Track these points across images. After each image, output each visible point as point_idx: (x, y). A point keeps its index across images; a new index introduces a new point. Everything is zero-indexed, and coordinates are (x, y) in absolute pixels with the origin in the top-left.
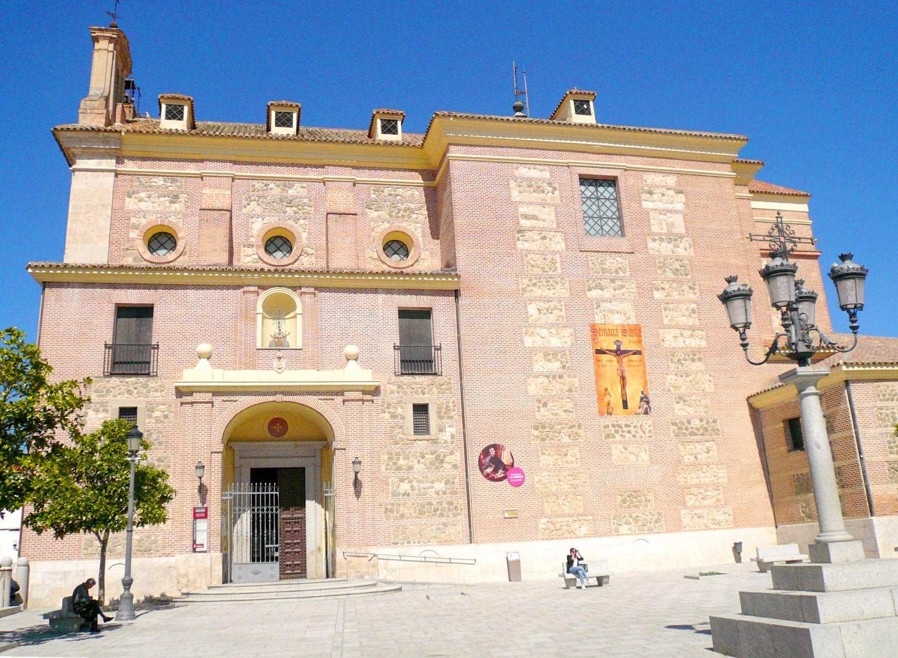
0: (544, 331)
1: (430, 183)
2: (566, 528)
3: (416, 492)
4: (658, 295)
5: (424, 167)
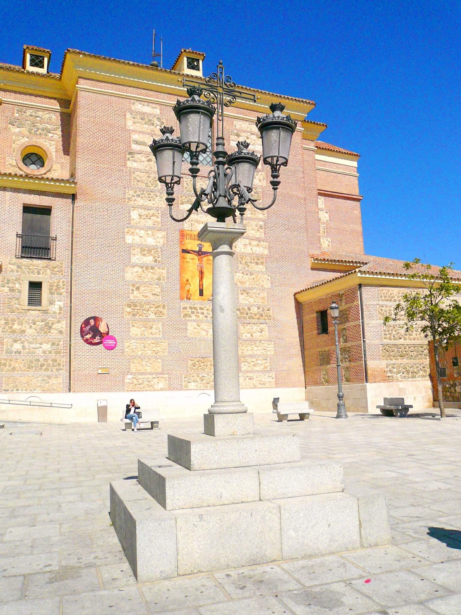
1: (65, 110)
2: (146, 383)
3: (27, 350)
5: (64, 97)
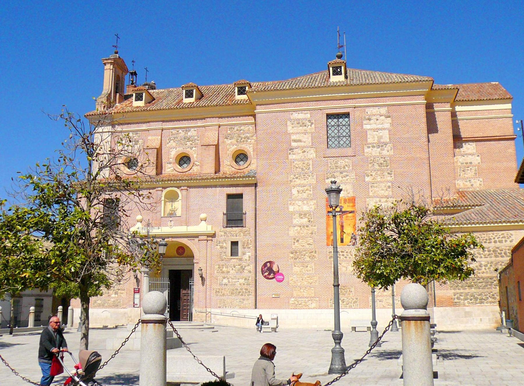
0: (300, 202)
4: (367, 179)
